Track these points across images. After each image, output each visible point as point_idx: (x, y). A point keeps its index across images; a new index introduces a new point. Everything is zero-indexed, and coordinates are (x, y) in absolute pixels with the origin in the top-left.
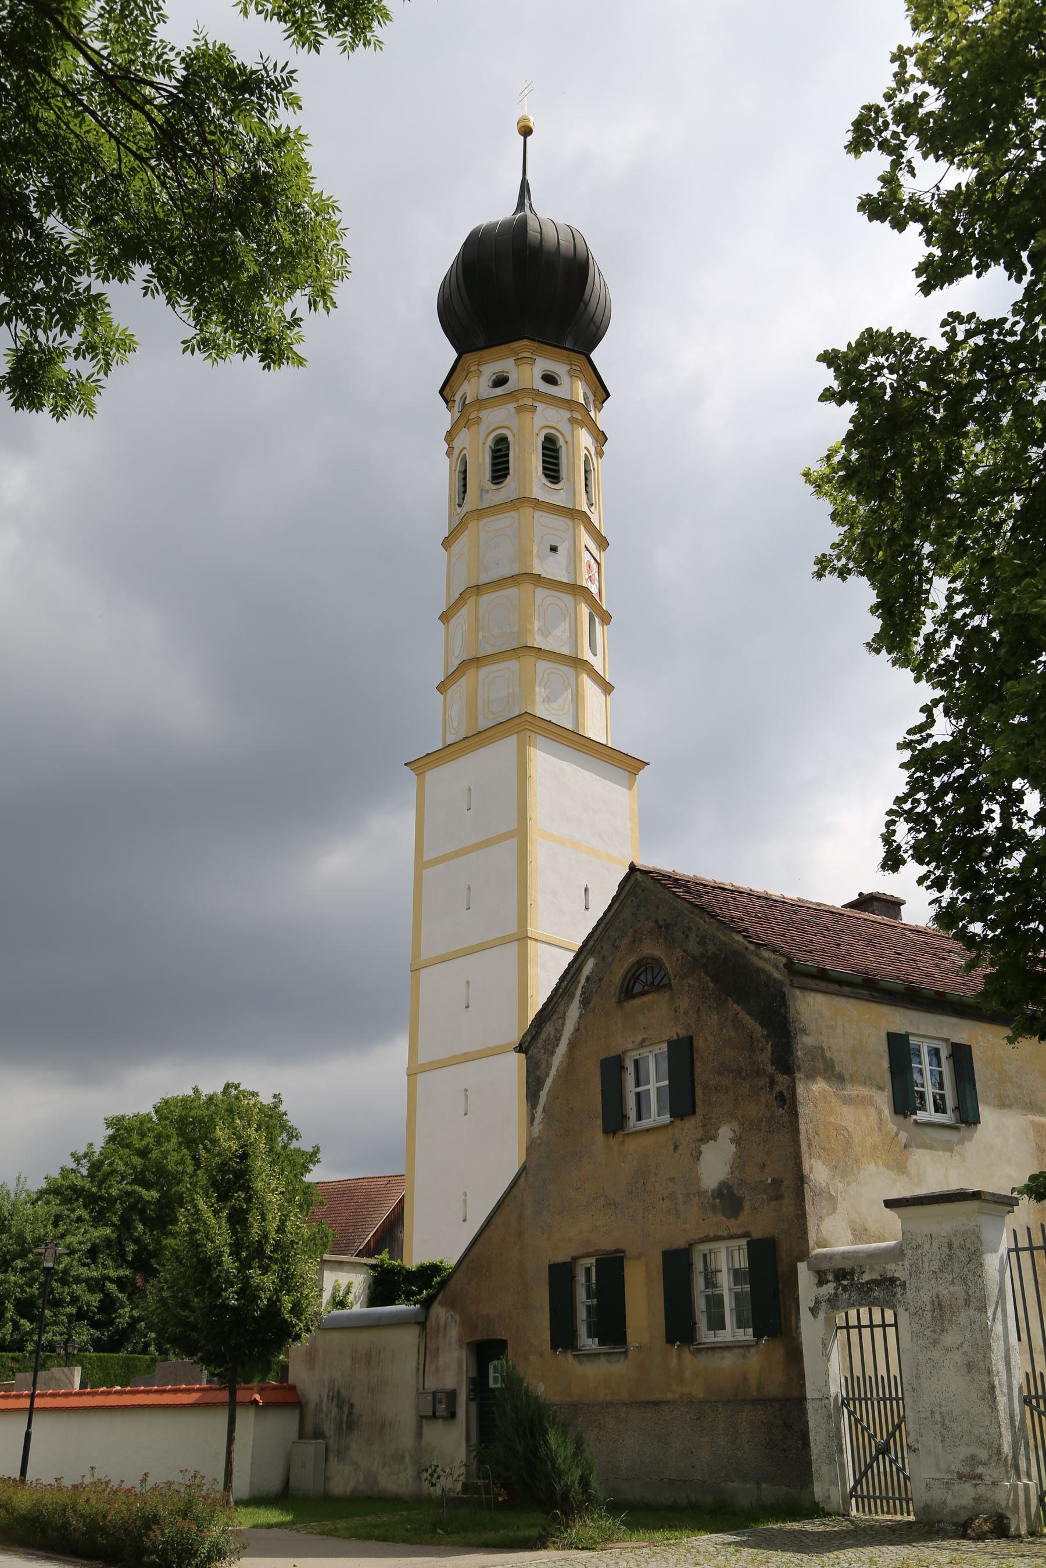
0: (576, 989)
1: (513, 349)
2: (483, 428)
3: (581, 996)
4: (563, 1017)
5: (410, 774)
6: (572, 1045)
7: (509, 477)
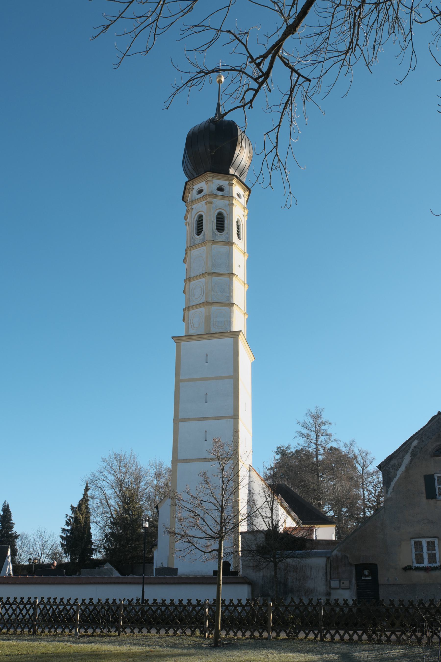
0: (409, 449)
1: (228, 178)
2: (194, 212)
3: (411, 452)
4: (402, 458)
6: (408, 469)
7: (203, 232)
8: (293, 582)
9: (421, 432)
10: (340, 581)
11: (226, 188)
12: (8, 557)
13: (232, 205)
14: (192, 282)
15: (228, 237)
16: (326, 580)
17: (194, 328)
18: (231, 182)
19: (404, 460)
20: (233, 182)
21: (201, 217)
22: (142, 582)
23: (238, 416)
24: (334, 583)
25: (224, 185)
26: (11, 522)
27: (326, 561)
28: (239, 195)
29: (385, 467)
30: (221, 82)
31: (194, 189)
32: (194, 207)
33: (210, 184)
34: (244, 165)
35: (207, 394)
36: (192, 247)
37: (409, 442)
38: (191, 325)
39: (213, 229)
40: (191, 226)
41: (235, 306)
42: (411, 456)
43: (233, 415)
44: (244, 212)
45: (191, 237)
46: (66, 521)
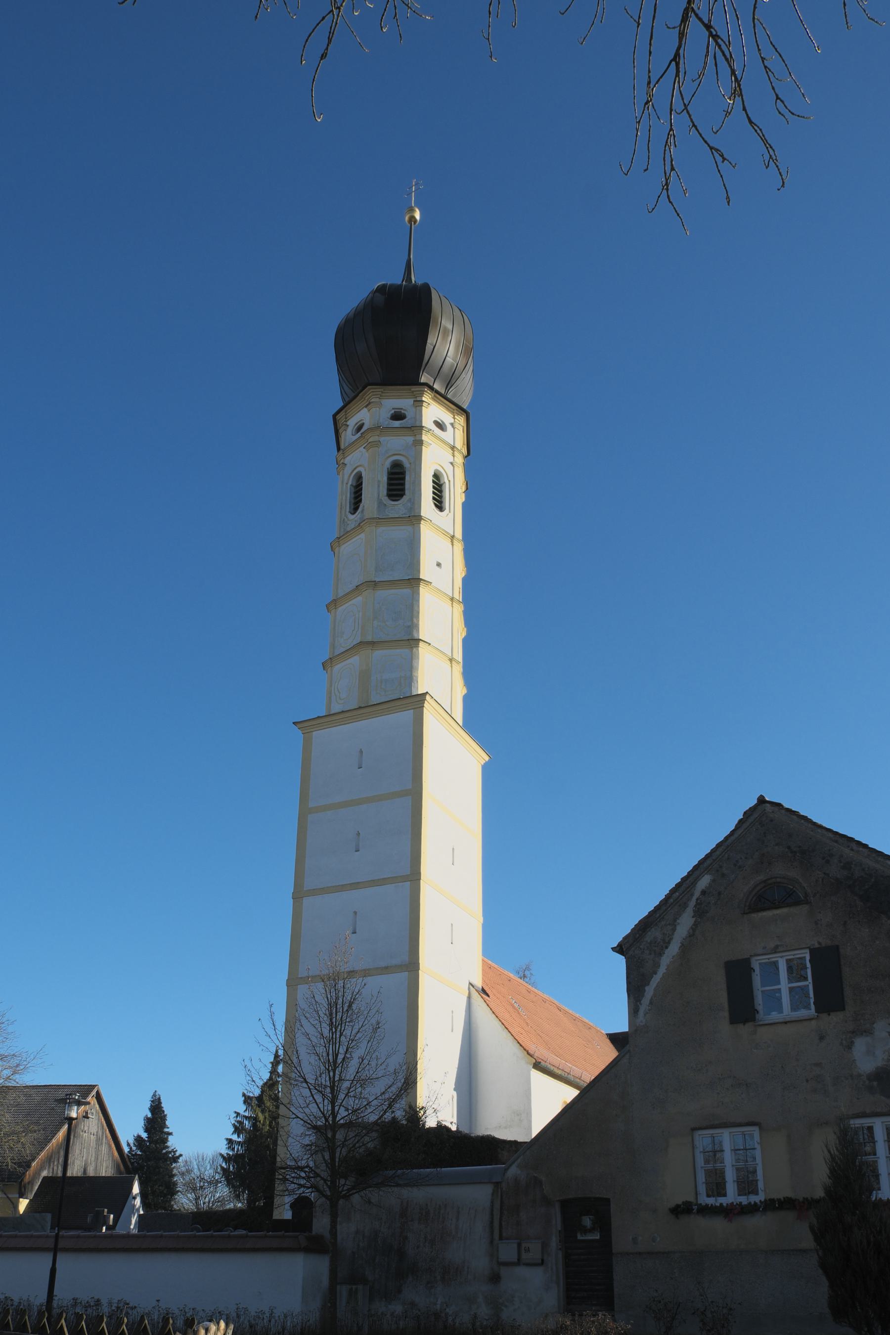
0: (689, 899)
1: (413, 392)
3: (695, 906)
4: (674, 925)
5: (298, 733)
6: (685, 948)
8: (418, 1247)
9: (718, 853)
10: (519, 1245)
11: (409, 414)
12: (134, 1198)
13: (420, 443)
14: (340, 609)
15: (411, 508)
16: (492, 1242)
17: (340, 699)
18: (418, 399)
19: (678, 928)
20: (424, 399)
21: (359, 478)
22: (52, 1246)
23: (419, 874)
24: (508, 1251)
25: (404, 408)
26: (166, 1130)
27: (493, 1194)
28: (440, 425)
29: (633, 949)
30: (415, 221)
31: (349, 427)
32: (347, 461)
33: (374, 409)
34: (452, 365)
35: (358, 834)
36: (341, 539)
37: (688, 881)
38: (336, 696)
39: (379, 496)
40: (342, 499)
41: (421, 644)
42: (693, 917)
43: (409, 873)
44: (454, 456)
45: (341, 519)
46: (234, 1125)
